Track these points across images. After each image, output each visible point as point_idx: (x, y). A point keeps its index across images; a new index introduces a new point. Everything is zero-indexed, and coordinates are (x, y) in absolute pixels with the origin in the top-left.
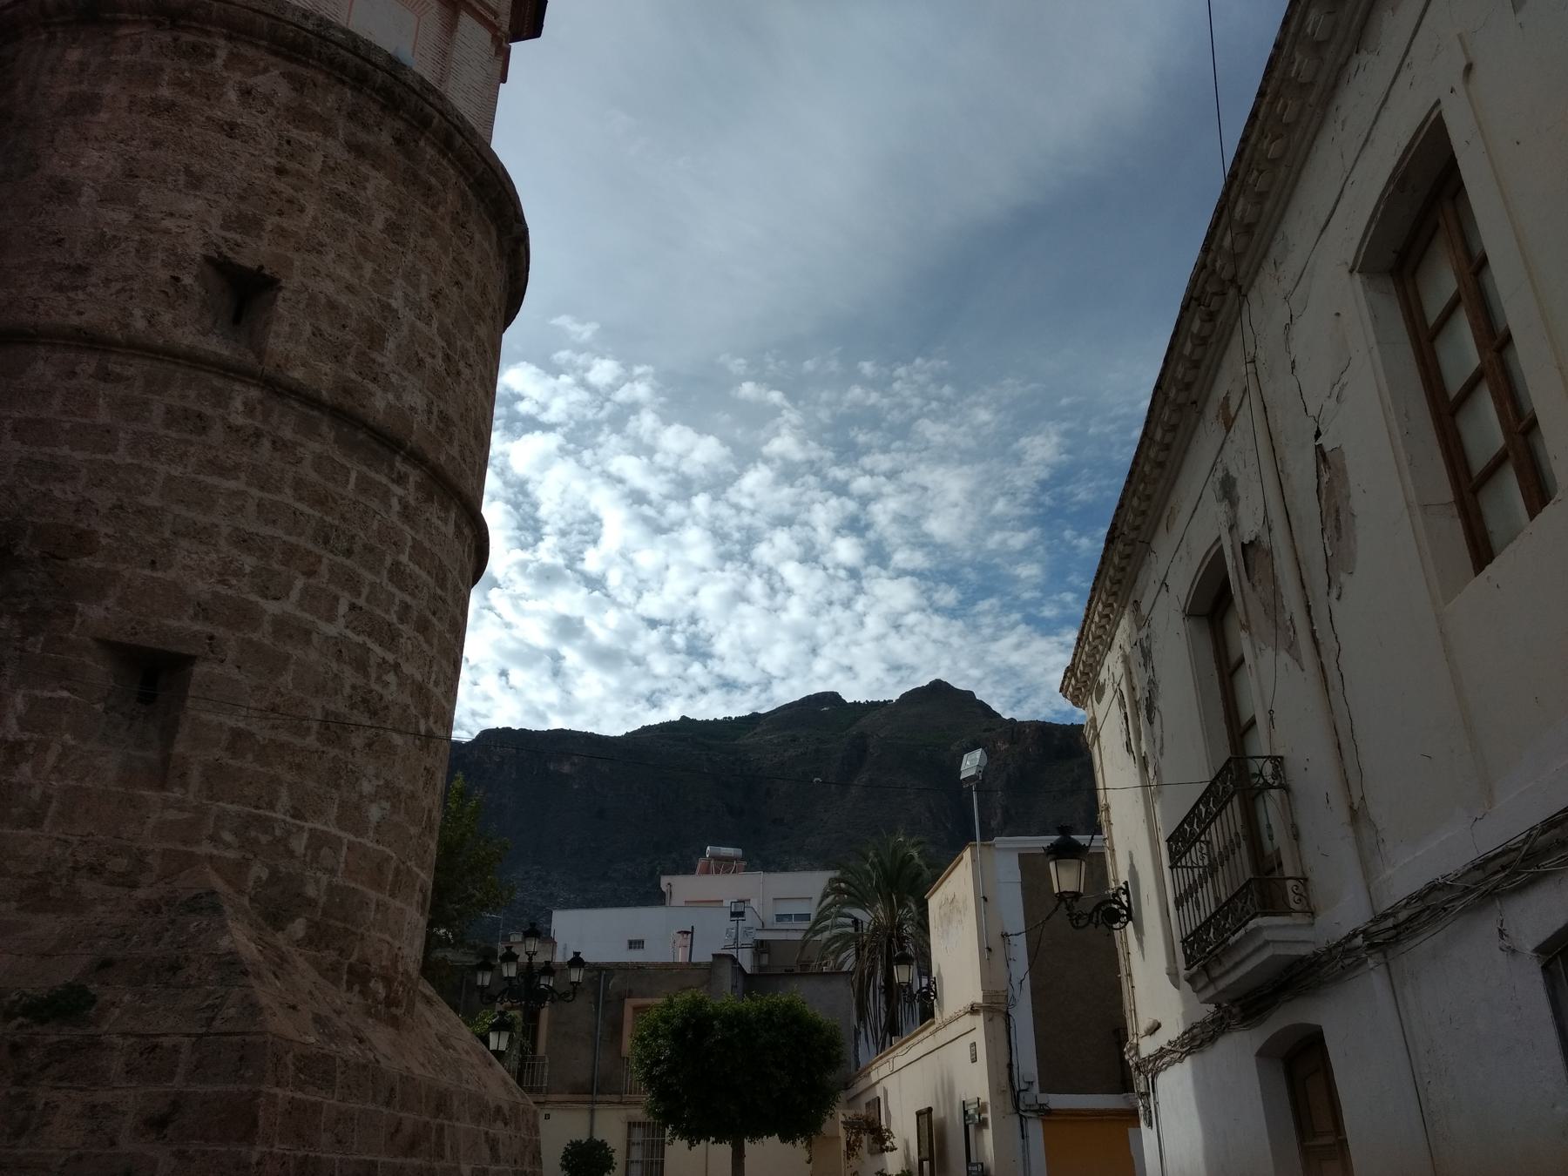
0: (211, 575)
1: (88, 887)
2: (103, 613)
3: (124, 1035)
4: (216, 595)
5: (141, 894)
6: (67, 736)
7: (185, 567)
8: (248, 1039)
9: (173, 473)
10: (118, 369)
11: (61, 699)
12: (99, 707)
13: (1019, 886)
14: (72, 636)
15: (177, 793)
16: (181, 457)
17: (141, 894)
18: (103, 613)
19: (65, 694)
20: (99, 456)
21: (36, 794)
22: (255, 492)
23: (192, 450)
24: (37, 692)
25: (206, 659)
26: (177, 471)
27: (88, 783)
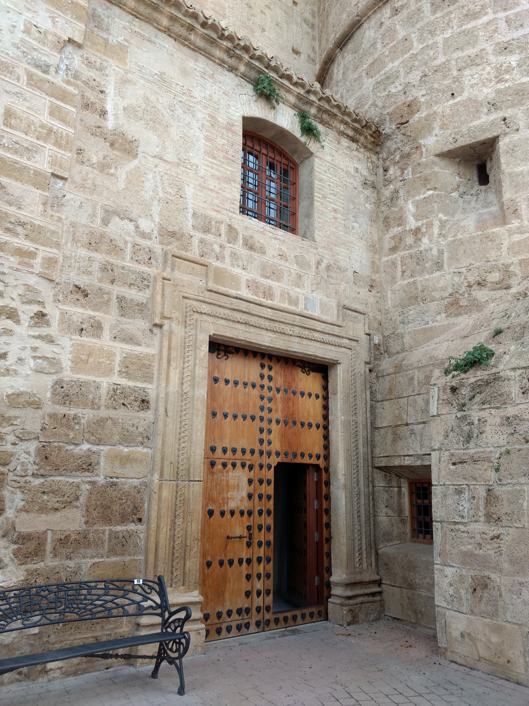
0: (491, 81)
1: (481, 295)
2: (435, 139)
3: (514, 369)
4: (498, 92)
5: (513, 291)
6: (441, 215)
7: (472, 86)
9: (447, 36)
11: (430, 196)
12: (455, 194)
14: (424, 160)
15: (515, 223)
16: (448, 24)
17: (513, 291)
18: (435, 139)
19: (431, 192)
20: (406, 56)
21: (435, 252)
22: (502, 15)
23: (453, 16)
24: (417, 198)
25: (506, 134)
26: (448, 34)
27: (459, 236)
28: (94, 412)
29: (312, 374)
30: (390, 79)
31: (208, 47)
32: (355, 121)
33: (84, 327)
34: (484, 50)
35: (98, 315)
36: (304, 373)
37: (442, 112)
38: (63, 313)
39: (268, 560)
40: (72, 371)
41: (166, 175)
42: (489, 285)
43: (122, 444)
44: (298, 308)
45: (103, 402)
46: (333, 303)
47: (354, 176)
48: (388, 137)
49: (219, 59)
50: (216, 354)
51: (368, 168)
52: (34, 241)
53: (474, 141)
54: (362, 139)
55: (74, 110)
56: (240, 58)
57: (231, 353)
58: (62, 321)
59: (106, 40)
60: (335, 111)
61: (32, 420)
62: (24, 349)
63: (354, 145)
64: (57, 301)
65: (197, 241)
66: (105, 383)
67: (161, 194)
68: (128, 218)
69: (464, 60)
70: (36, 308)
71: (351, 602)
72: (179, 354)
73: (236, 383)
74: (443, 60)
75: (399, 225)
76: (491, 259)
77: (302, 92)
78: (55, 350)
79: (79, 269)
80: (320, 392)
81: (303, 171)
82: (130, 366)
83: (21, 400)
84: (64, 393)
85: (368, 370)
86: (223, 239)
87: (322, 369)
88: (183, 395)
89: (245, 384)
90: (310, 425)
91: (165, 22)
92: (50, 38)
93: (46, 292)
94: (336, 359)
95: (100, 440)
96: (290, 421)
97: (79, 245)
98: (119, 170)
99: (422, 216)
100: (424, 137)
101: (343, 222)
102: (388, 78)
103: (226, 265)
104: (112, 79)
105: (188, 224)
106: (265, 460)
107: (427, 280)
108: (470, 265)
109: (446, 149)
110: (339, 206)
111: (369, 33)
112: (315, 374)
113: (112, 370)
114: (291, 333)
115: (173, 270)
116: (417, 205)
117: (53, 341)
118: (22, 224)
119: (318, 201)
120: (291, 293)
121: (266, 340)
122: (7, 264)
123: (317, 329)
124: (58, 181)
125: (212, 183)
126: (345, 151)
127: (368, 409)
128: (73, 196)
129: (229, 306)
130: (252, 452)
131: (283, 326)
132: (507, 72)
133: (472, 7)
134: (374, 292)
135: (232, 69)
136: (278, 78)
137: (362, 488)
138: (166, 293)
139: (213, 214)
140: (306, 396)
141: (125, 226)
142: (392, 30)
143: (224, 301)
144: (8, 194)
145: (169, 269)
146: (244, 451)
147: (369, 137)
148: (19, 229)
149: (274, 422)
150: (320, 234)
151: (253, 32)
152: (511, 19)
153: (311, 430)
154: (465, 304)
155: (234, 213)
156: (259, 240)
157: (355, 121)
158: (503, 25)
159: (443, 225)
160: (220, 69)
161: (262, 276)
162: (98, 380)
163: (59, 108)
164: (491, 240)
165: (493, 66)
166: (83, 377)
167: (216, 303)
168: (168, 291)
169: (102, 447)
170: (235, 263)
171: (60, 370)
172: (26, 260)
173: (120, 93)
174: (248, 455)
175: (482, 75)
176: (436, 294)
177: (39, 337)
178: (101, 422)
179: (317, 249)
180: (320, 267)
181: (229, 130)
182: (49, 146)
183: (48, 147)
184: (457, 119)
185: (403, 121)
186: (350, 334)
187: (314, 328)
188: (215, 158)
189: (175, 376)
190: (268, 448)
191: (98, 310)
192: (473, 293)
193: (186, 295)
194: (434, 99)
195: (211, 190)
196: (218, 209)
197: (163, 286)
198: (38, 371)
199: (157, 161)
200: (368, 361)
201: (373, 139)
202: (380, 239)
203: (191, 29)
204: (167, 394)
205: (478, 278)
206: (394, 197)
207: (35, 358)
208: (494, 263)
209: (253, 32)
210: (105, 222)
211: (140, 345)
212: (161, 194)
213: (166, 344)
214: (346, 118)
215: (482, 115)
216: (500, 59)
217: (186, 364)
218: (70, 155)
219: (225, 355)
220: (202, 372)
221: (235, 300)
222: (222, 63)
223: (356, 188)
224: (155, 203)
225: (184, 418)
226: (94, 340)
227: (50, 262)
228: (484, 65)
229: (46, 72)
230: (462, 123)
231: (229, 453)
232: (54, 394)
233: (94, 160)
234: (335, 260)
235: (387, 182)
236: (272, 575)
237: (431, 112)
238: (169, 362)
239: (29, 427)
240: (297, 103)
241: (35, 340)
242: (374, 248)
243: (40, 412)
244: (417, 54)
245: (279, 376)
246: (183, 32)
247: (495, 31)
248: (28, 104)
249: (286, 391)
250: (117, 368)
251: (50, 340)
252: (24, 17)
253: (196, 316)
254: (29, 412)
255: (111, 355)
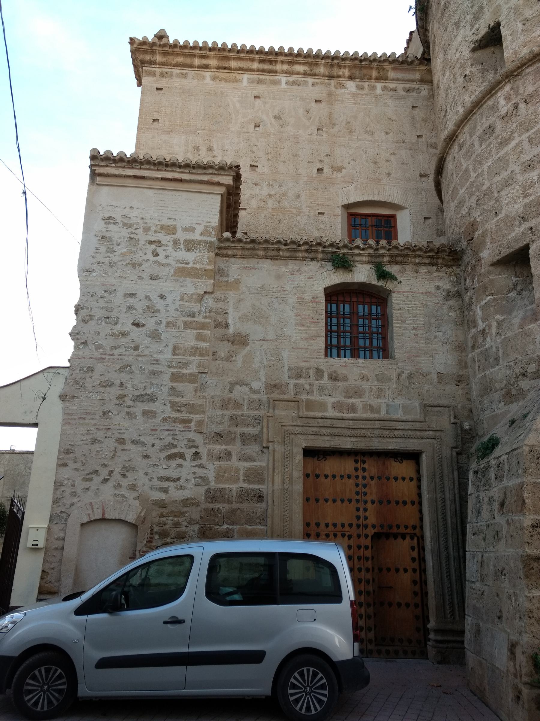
0: (519, 197)
1: (525, 384)
4: (525, 206)
6: (498, 316)
7: (507, 204)
8: (518, 450)
9: (489, 164)
10: (462, 140)
11: (489, 301)
13: (78, 682)
16: (489, 153)
19: (488, 298)
20: (468, 184)
21: (494, 349)
22: (525, 136)
23: (492, 146)
28: (229, 505)
29: (405, 462)
30: (461, 204)
31: (293, 254)
32: (426, 252)
33: (221, 456)
34: (514, 171)
35: (229, 448)
36: (397, 462)
37: (491, 229)
38: (209, 450)
39: (369, 605)
40: (215, 483)
41: (269, 350)
42: (529, 375)
43: (247, 524)
44: (380, 414)
45: (234, 499)
46: (417, 404)
47: (435, 294)
48: (463, 251)
49: (302, 258)
50: (316, 457)
51: (451, 282)
52: (191, 413)
53: (512, 250)
54: (440, 261)
55: (209, 332)
56: (317, 251)
57: (328, 455)
58: (208, 455)
59: (227, 281)
60: (406, 252)
61: (195, 513)
62: (189, 473)
63: (435, 268)
64: (205, 443)
65: (292, 386)
66: (235, 487)
67: (266, 363)
68: (244, 385)
69: (501, 183)
70: (194, 450)
71: (441, 645)
72: (280, 464)
73: (334, 477)
74: (488, 185)
75: (474, 327)
76: (529, 353)
77: (371, 251)
78: (205, 472)
79: (217, 422)
80: (413, 475)
81: (389, 304)
82: (250, 475)
83: (189, 502)
84: (212, 496)
85: (454, 454)
86: (311, 379)
87: (414, 457)
88: (284, 491)
89: (342, 477)
90: (405, 503)
91: (262, 253)
92: (194, 297)
93: (198, 439)
94: (418, 449)
95: (233, 522)
96: (384, 501)
97: (216, 408)
98: (238, 357)
99: (485, 319)
100: (482, 251)
101: (424, 335)
102: (460, 202)
103: (316, 396)
104: (231, 304)
105: (285, 376)
106: (362, 531)
107: (491, 373)
108: (516, 358)
109: (495, 260)
110: (420, 324)
111: (450, 165)
112: (409, 461)
113: (238, 479)
114: (372, 435)
115: (274, 409)
116: (483, 308)
117: (204, 467)
118: (184, 406)
119: (397, 327)
120: (373, 404)
121: (348, 444)
122: (177, 429)
123: (398, 428)
124: (203, 375)
125: (302, 344)
126: (424, 276)
127: (456, 487)
128: (211, 381)
129: (317, 425)
130: (351, 525)
131: (364, 431)
132: (531, 186)
133: (504, 135)
134: (462, 386)
135: (313, 259)
136: (348, 251)
137: (452, 553)
138: (270, 425)
139: (304, 364)
140: (400, 481)
141: (243, 390)
142: (459, 163)
143: (312, 422)
144: (177, 391)
145: (271, 410)
146: (343, 525)
147: (447, 257)
148: (183, 409)
149: (369, 502)
150: (401, 351)
151: (380, 180)
152: (532, 138)
153: (406, 506)
154: (515, 393)
155: (320, 358)
156: (342, 371)
157: (426, 252)
158: (526, 145)
159: (500, 324)
160: (305, 263)
161: (345, 397)
162: (230, 486)
163: (200, 334)
164: (528, 336)
165: (520, 184)
166: (222, 486)
167: (306, 425)
168: (271, 424)
169: (235, 527)
170: (322, 393)
171: (208, 483)
172: (187, 425)
173: (236, 309)
174: (347, 528)
175: (513, 193)
176: (497, 386)
177: (196, 466)
178: (233, 512)
179: (397, 364)
180: (401, 378)
181: (315, 302)
182: (197, 358)
183: (195, 359)
184: (499, 233)
185: (470, 238)
186: (434, 426)
187: (394, 428)
188: (303, 326)
189: (278, 479)
190: (364, 522)
191: (229, 445)
192: (519, 383)
193: (283, 424)
194: (485, 218)
195: (301, 348)
196: (308, 360)
197: (268, 422)
198: (196, 485)
199: (262, 342)
200: (455, 446)
201: (451, 258)
202: (466, 339)
203: (279, 249)
204: (273, 491)
205: (522, 370)
206: (470, 304)
207: (195, 478)
208: (532, 356)
209: (380, 180)
210: (231, 391)
211: (255, 462)
212: (266, 363)
213: (271, 459)
214: (418, 253)
215: (516, 228)
216: (525, 177)
217: (286, 470)
218: (208, 358)
219: (324, 458)
220: (298, 474)
221: (321, 420)
222: (305, 259)
223: (438, 303)
224: (262, 369)
225: (286, 505)
226: (227, 463)
227: (200, 423)
228: (514, 184)
229: (194, 317)
230: (503, 236)
231: (331, 527)
232: (206, 497)
233: (223, 355)
234: (417, 369)
235: (467, 290)
236: (364, 616)
237: (484, 230)
238: (274, 470)
239: (193, 517)
240: (370, 259)
241: (195, 468)
242: (461, 348)
243: (199, 508)
244: (473, 182)
245: (372, 467)
246: (274, 253)
247: (521, 152)
248: (184, 339)
249: (379, 478)
250: (242, 478)
251: (202, 467)
252: (179, 292)
253: (292, 436)
254: (194, 508)
255: (237, 470)
